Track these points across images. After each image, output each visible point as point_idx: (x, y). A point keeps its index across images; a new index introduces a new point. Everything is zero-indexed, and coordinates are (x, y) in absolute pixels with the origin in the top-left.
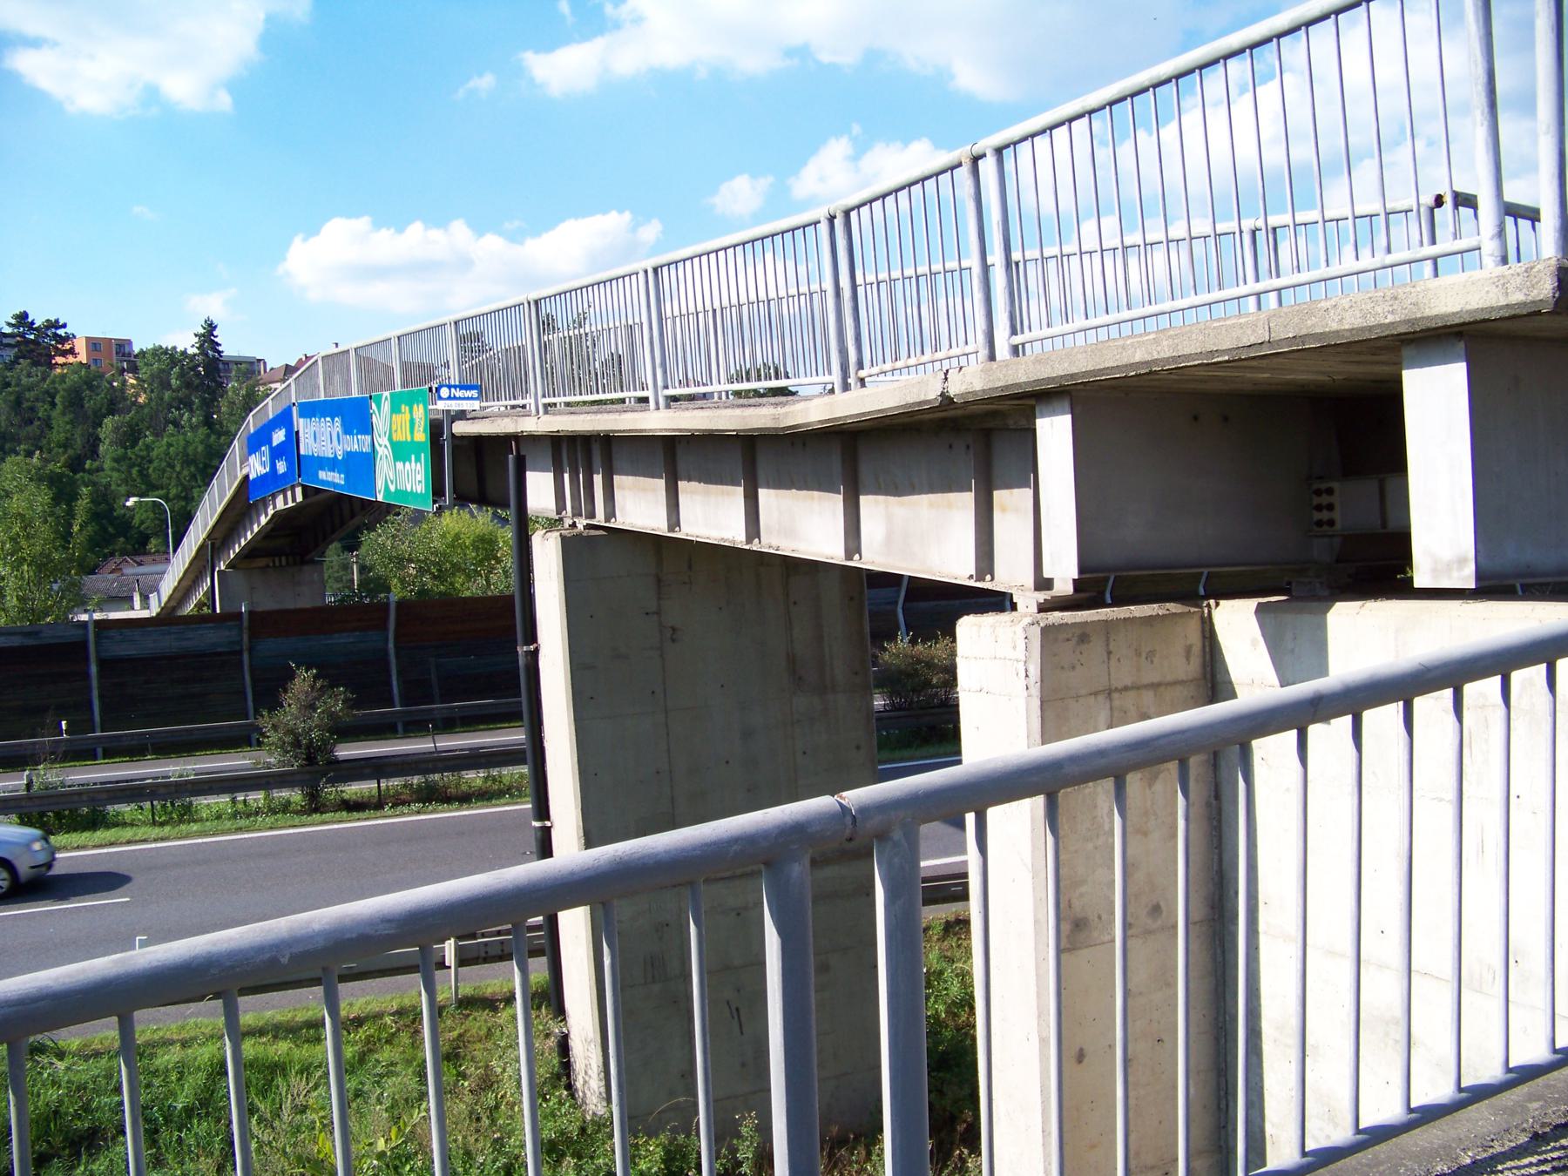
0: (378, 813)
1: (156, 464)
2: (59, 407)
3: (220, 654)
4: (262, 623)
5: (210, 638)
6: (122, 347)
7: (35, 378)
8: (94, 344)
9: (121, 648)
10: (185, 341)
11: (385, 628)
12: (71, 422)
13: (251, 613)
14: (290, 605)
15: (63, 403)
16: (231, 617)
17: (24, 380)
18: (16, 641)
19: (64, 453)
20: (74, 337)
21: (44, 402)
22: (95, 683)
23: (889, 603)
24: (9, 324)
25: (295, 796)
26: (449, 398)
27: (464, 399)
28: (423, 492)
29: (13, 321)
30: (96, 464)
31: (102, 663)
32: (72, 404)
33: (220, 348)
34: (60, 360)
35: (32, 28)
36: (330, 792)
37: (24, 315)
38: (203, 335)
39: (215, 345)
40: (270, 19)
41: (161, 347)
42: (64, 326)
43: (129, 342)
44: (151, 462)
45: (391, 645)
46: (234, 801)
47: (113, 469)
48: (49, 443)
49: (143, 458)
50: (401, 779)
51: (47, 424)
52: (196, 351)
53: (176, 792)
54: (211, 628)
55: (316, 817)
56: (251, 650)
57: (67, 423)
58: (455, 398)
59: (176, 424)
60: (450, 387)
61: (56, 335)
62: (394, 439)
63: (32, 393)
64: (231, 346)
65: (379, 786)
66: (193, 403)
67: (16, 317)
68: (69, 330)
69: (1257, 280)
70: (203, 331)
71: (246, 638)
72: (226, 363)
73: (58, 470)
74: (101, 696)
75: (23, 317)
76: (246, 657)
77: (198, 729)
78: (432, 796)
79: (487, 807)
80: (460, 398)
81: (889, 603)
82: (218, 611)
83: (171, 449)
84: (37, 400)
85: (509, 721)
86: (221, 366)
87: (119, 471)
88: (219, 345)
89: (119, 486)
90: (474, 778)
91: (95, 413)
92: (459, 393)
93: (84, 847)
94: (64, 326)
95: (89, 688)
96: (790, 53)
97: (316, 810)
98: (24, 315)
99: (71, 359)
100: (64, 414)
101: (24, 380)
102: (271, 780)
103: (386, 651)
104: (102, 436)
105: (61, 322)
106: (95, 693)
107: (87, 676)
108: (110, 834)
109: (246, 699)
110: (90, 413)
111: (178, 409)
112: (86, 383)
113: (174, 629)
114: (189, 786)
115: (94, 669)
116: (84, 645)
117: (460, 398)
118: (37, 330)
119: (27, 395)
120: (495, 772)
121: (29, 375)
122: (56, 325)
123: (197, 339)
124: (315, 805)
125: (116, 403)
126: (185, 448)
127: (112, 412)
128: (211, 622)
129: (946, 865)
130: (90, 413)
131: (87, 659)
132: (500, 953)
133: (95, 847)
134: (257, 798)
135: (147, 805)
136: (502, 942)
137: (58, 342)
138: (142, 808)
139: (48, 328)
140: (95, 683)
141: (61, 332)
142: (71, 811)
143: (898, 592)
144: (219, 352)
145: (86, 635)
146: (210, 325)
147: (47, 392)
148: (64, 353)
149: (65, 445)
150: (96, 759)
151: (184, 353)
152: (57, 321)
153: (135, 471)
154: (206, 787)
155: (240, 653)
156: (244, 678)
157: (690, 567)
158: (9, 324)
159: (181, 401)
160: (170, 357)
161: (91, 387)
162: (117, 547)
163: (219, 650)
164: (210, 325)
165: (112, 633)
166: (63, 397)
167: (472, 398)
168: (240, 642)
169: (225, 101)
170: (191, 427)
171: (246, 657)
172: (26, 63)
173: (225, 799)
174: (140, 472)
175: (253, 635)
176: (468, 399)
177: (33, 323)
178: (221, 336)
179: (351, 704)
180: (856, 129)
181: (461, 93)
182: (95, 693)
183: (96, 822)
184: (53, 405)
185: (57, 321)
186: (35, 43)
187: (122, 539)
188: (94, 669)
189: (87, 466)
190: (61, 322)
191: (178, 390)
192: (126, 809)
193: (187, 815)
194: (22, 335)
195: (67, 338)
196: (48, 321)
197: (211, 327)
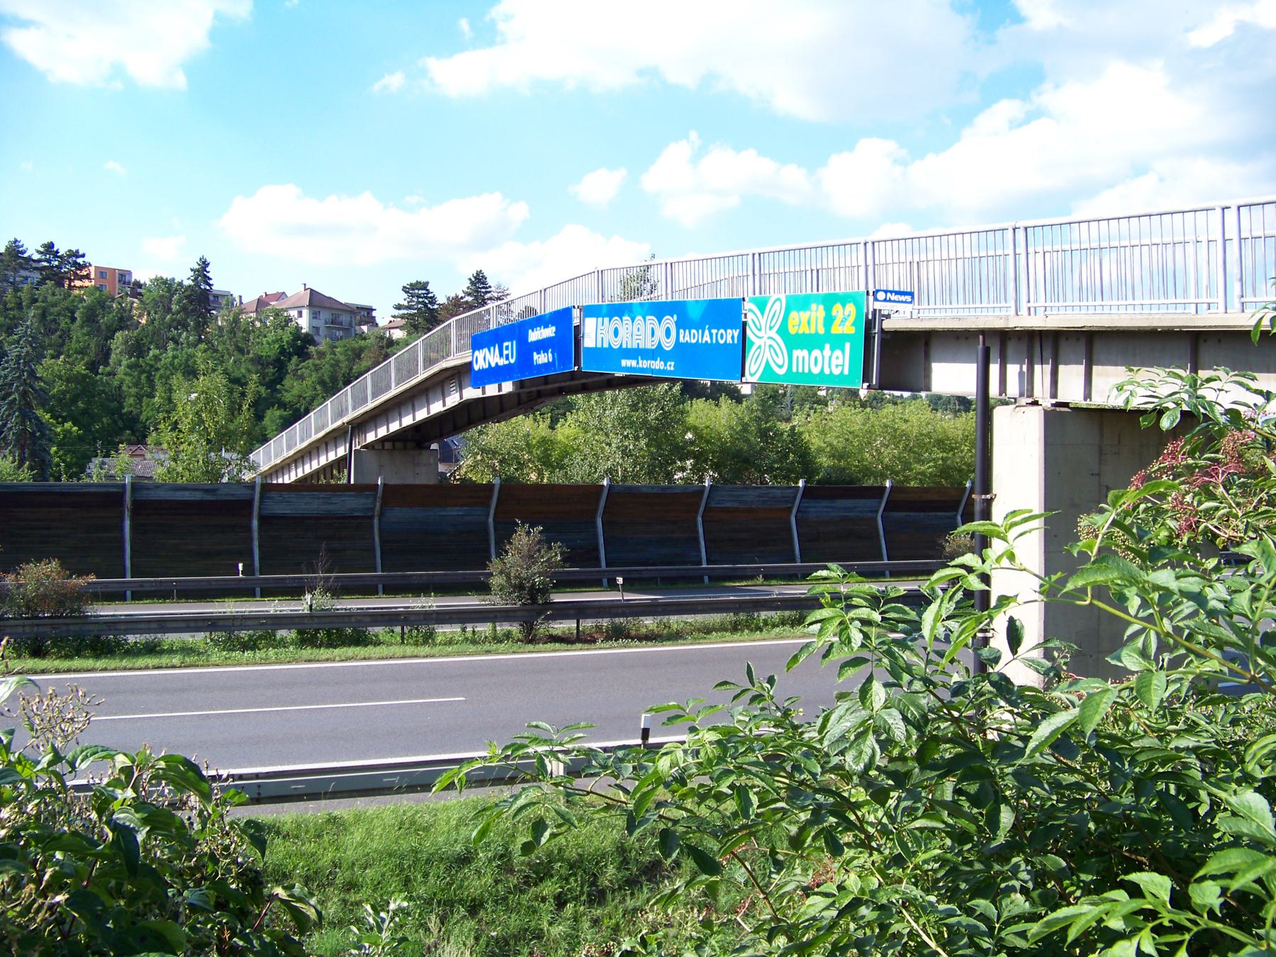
0: (593, 646)
1: (162, 371)
2: (79, 322)
3: (358, 517)
4: (393, 494)
5: (351, 504)
6: (123, 276)
7: (58, 297)
8: (102, 272)
9: (279, 508)
10: (184, 276)
11: (489, 506)
12: (88, 334)
13: (385, 485)
14: (410, 481)
15: (82, 317)
16: (363, 489)
17: (50, 298)
18: (198, 496)
19: (82, 359)
20: (90, 265)
21: (65, 316)
22: (256, 535)
23: (872, 512)
24: (38, 252)
25: (515, 628)
26: (885, 300)
27: (899, 302)
28: (846, 372)
29: (42, 250)
30: (108, 369)
31: (263, 519)
32: (88, 320)
33: (211, 282)
34: (78, 283)
35: (25, 12)
36: (542, 628)
37: (51, 245)
38: (198, 270)
39: (207, 279)
40: (217, 16)
41: (162, 278)
42: (83, 256)
43: (130, 273)
44: (157, 369)
45: (491, 520)
46: (464, 630)
47: (126, 374)
48: (68, 350)
49: (151, 366)
50: (594, 620)
51: (66, 335)
52: (192, 283)
53: (425, 619)
54: (352, 496)
55: (530, 647)
56: (381, 515)
57: (85, 335)
58: (890, 301)
59: (176, 342)
60: (886, 292)
61: (75, 263)
62: (792, 331)
63: (56, 309)
64: (219, 283)
65: (578, 627)
66: (189, 325)
67: (44, 246)
68: (86, 259)
69: (760, 293)
70: (197, 267)
71: (378, 504)
72: (216, 296)
73: (83, 372)
74: (260, 547)
75: (49, 246)
76: (376, 521)
77: (346, 577)
78: (618, 634)
79: (673, 645)
80: (894, 301)
81: (872, 512)
82: (352, 482)
83: (176, 361)
84: (59, 314)
85: (591, 586)
86: (211, 298)
87: (131, 375)
88: (210, 279)
89: (129, 387)
90: (649, 622)
91: (108, 327)
92: (894, 297)
93: (369, 659)
94: (83, 256)
95: (251, 539)
96: (641, 73)
97: (530, 642)
98: (51, 245)
99: (87, 283)
100: (82, 327)
101: (50, 298)
102: (498, 615)
103: (486, 523)
104: (113, 347)
105: (81, 253)
106: (256, 543)
107: (249, 528)
108: (370, 650)
109: (375, 557)
110: (103, 327)
111: (176, 329)
112: (99, 302)
113: (322, 495)
114: (434, 616)
115: (255, 523)
116: (250, 503)
117: (894, 301)
118: (61, 257)
119: (52, 310)
120: (665, 619)
121: (54, 294)
122: (76, 254)
123: (192, 273)
124: (530, 638)
125: (124, 321)
126: (187, 360)
127: (121, 328)
128: (325, 491)
129: (407, 756)
130: (103, 327)
131: (251, 514)
132: (257, 796)
133: (379, 659)
134: (484, 629)
135: (398, 629)
136: (259, 785)
137: (77, 269)
138: (393, 631)
139: (69, 256)
140: (256, 535)
141: (80, 261)
142: (337, 630)
143: (880, 503)
144: (210, 285)
145: (253, 495)
146: (204, 262)
147: (67, 308)
148: (81, 278)
149: (82, 352)
150: (254, 596)
151: (180, 284)
152: (77, 251)
153: (143, 376)
154: (447, 617)
155: (372, 517)
156: (374, 539)
157: (1119, 442)
158: (38, 252)
159: (179, 323)
160: (166, 285)
161: (103, 308)
162: (123, 438)
163: (356, 514)
164: (204, 262)
165: (274, 494)
166: (82, 313)
167: (906, 302)
168: (373, 509)
169: (181, 81)
170: (188, 343)
171: (376, 521)
172: (20, 41)
173: (457, 628)
174: (148, 378)
175: (385, 503)
176: (902, 302)
177: (57, 252)
178: (212, 272)
179: (567, 559)
180: (693, 135)
181: (377, 87)
182: (256, 543)
183: (360, 640)
184: (73, 319)
185: (77, 251)
186: (24, 24)
187: (128, 432)
188: (255, 523)
189: (100, 371)
190: (81, 253)
191: (178, 312)
192: (379, 631)
193: (429, 638)
194: (49, 261)
195: (81, 267)
196: (70, 251)
197: (204, 264)
